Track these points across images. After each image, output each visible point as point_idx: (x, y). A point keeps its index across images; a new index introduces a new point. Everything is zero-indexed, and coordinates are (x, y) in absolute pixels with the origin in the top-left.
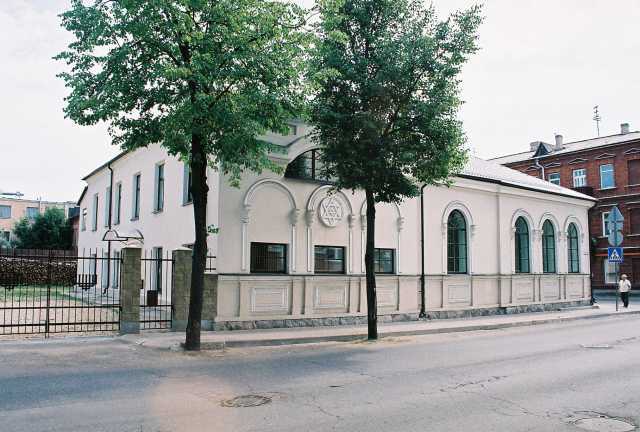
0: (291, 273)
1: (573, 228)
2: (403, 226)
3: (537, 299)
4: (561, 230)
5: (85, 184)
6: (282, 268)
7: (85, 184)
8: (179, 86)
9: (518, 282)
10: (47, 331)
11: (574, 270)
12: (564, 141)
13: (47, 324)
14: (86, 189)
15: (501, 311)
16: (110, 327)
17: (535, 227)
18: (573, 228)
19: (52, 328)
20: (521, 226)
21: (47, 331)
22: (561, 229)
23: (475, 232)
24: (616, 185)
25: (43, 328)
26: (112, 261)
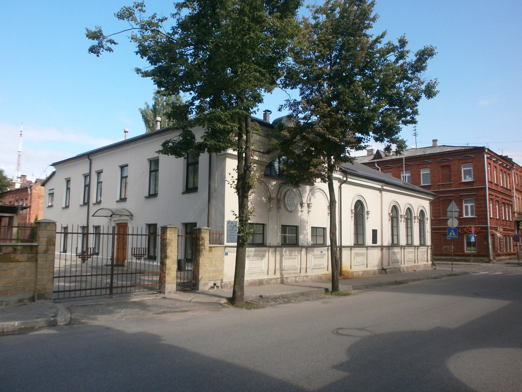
0: (268, 244)
1: (422, 213)
2: (311, 209)
3: (303, 271)
4: (416, 215)
5: (53, 169)
6: (295, 242)
7: (53, 169)
8: (205, 71)
9: (421, 250)
10: (111, 293)
11: (422, 244)
12: (439, 144)
13: (111, 288)
14: (54, 174)
15: (384, 272)
16: (104, 292)
17: (402, 211)
18: (422, 213)
19: (115, 291)
20: (395, 209)
21: (111, 293)
22: (416, 213)
23: (369, 216)
24: (432, 182)
25: (108, 292)
26: (116, 236)
